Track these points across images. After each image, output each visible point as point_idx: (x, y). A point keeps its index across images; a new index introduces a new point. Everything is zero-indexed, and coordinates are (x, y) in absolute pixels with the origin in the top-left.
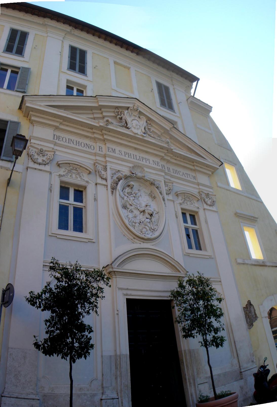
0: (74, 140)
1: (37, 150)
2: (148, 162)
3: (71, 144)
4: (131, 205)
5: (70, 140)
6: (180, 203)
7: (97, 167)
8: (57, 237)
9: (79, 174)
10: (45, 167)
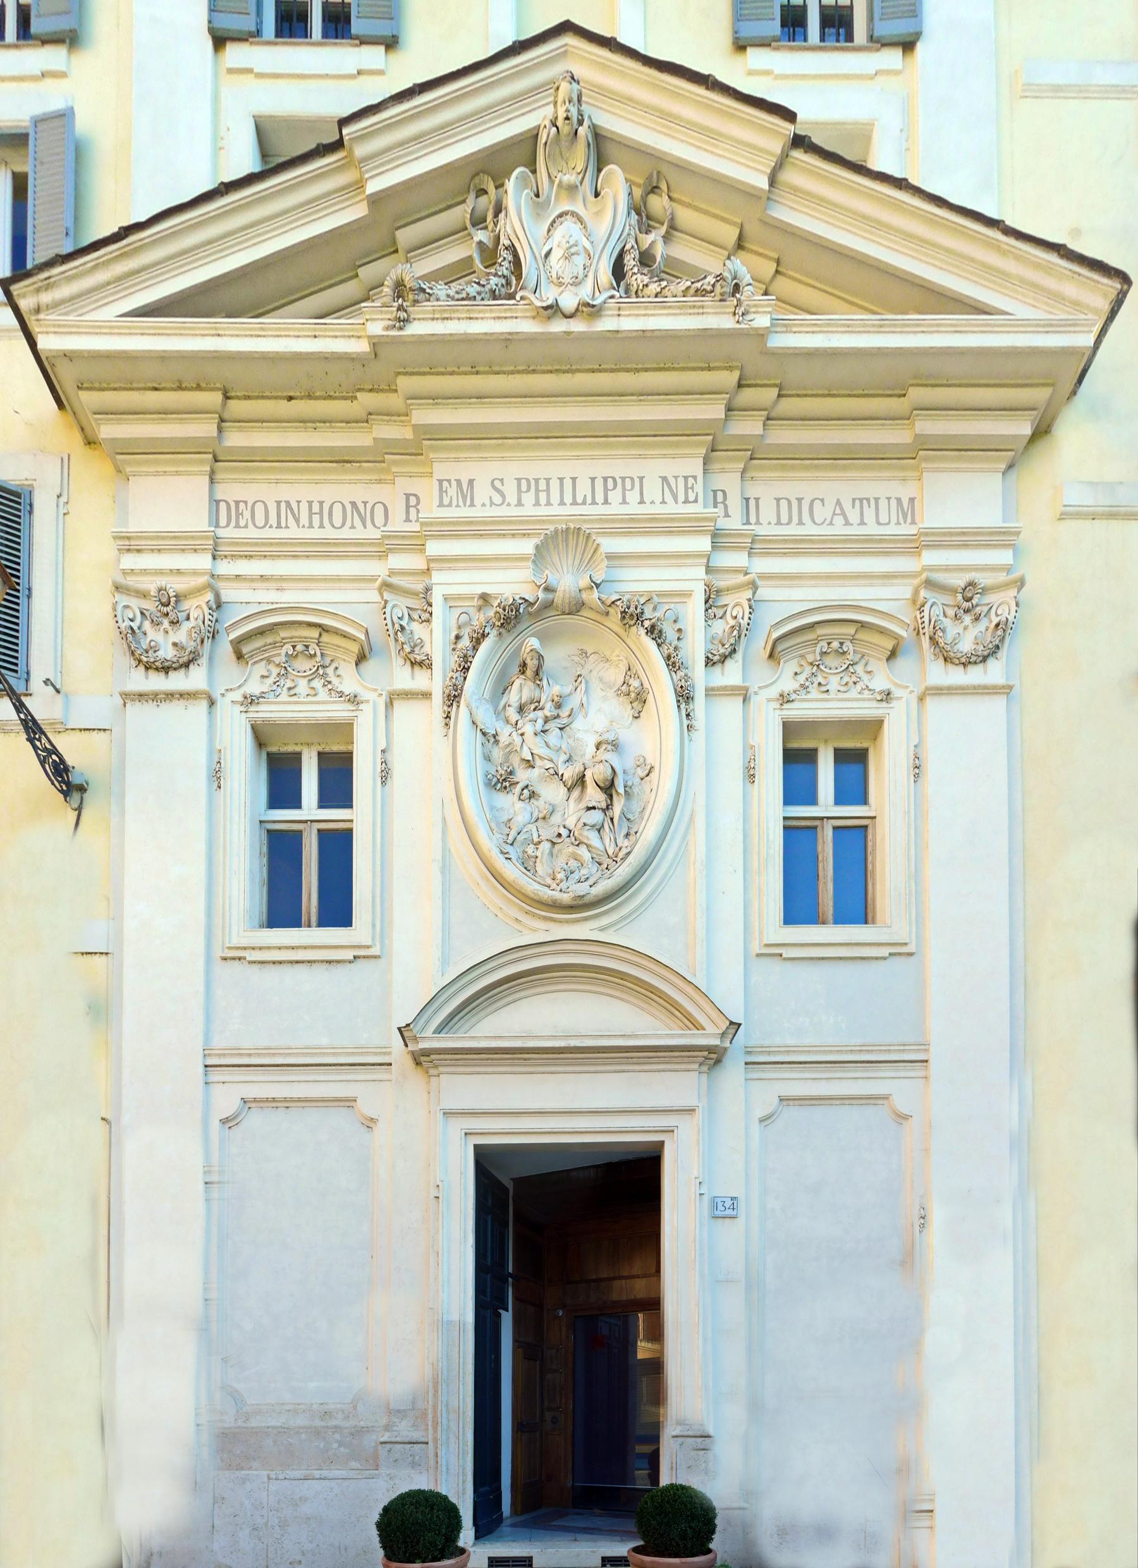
0: (299, 502)
1: (948, 599)
2: (633, 496)
3: (287, 527)
4: (530, 764)
5: (283, 505)
6: (781, 695)
7: (926, 608)
8: (784, 956)
9: (321, 671)
10: (187, 676)
